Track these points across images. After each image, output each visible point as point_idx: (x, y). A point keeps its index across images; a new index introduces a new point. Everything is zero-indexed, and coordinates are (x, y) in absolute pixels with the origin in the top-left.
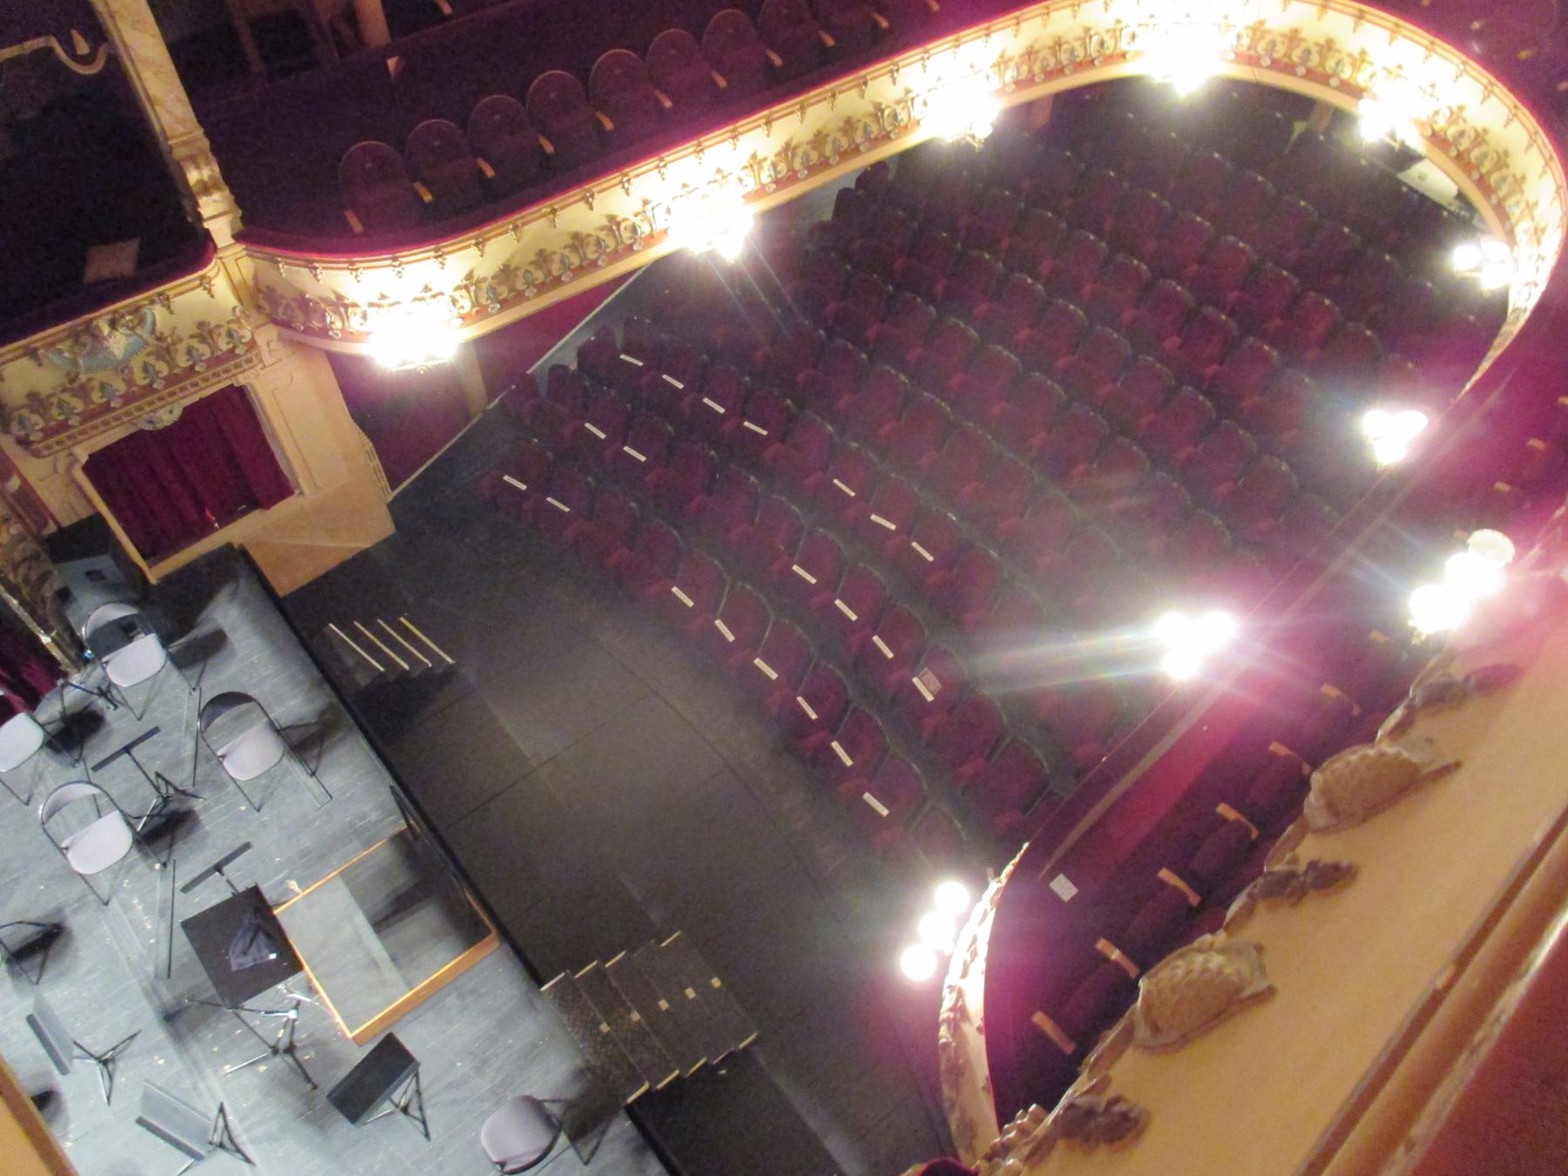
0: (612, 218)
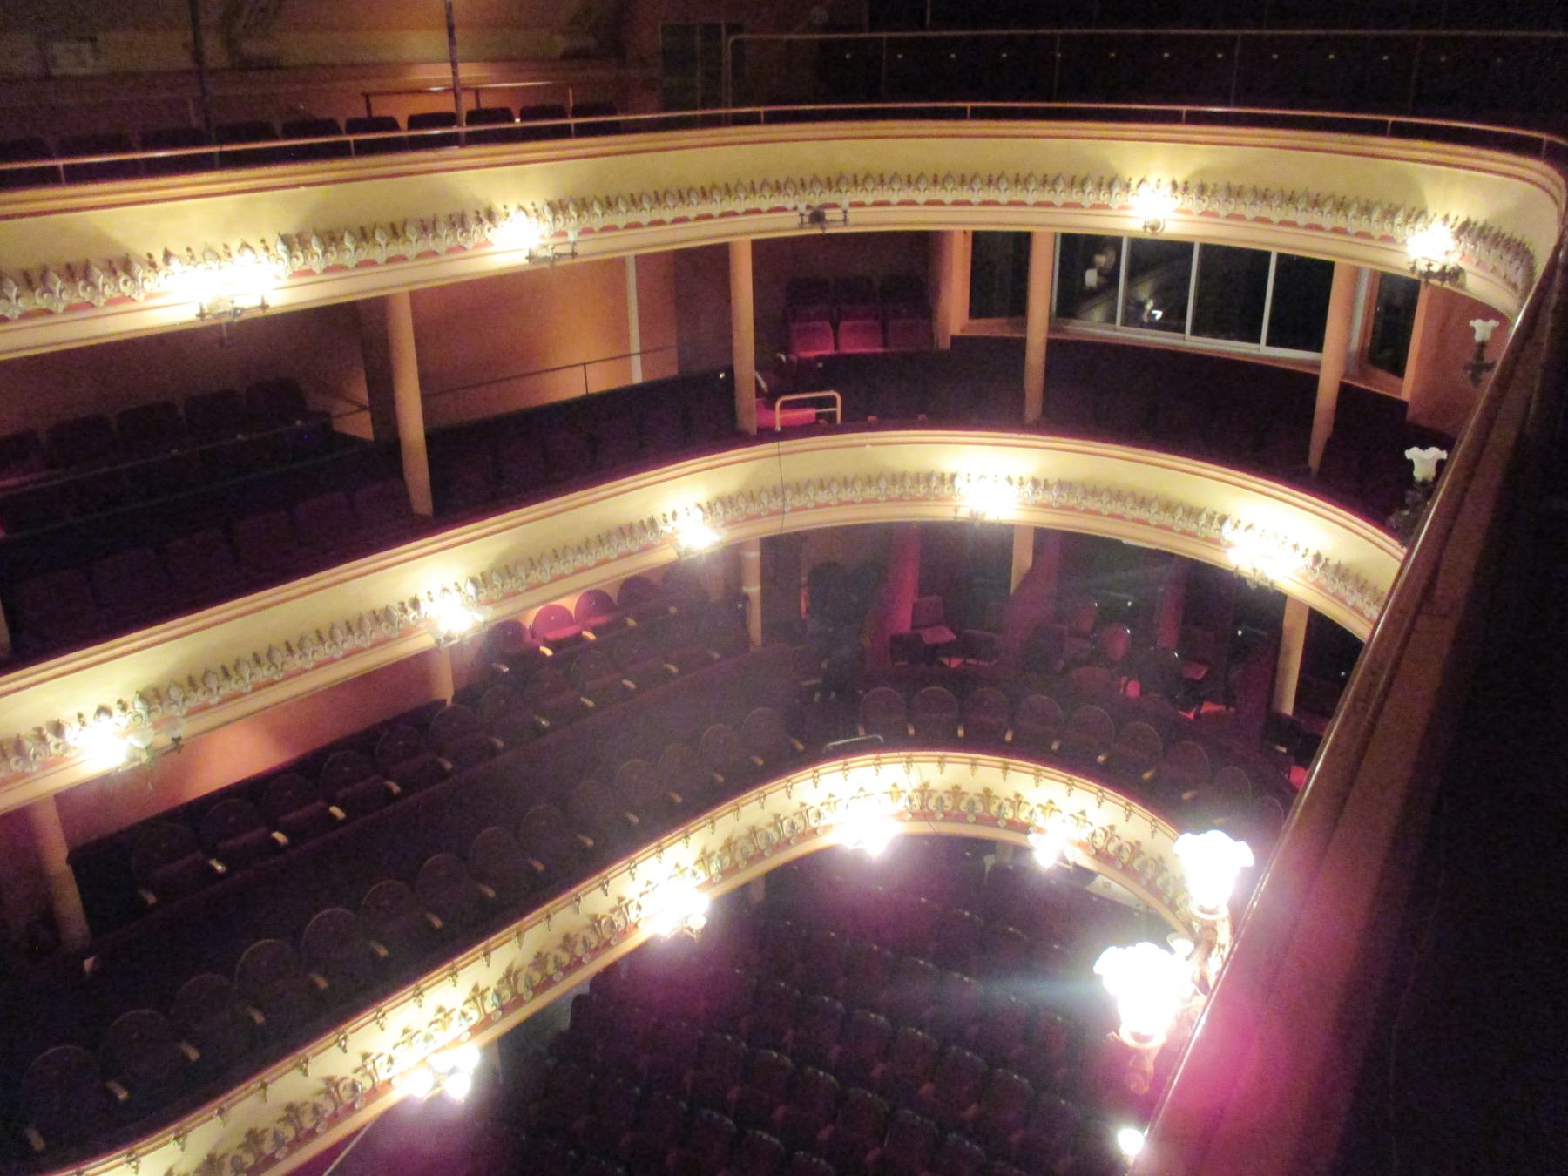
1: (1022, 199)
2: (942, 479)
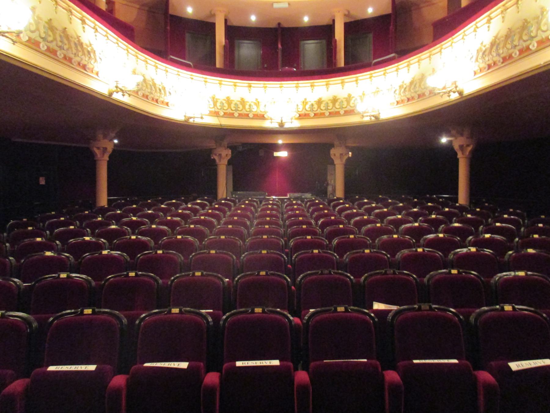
0: (349, 96)
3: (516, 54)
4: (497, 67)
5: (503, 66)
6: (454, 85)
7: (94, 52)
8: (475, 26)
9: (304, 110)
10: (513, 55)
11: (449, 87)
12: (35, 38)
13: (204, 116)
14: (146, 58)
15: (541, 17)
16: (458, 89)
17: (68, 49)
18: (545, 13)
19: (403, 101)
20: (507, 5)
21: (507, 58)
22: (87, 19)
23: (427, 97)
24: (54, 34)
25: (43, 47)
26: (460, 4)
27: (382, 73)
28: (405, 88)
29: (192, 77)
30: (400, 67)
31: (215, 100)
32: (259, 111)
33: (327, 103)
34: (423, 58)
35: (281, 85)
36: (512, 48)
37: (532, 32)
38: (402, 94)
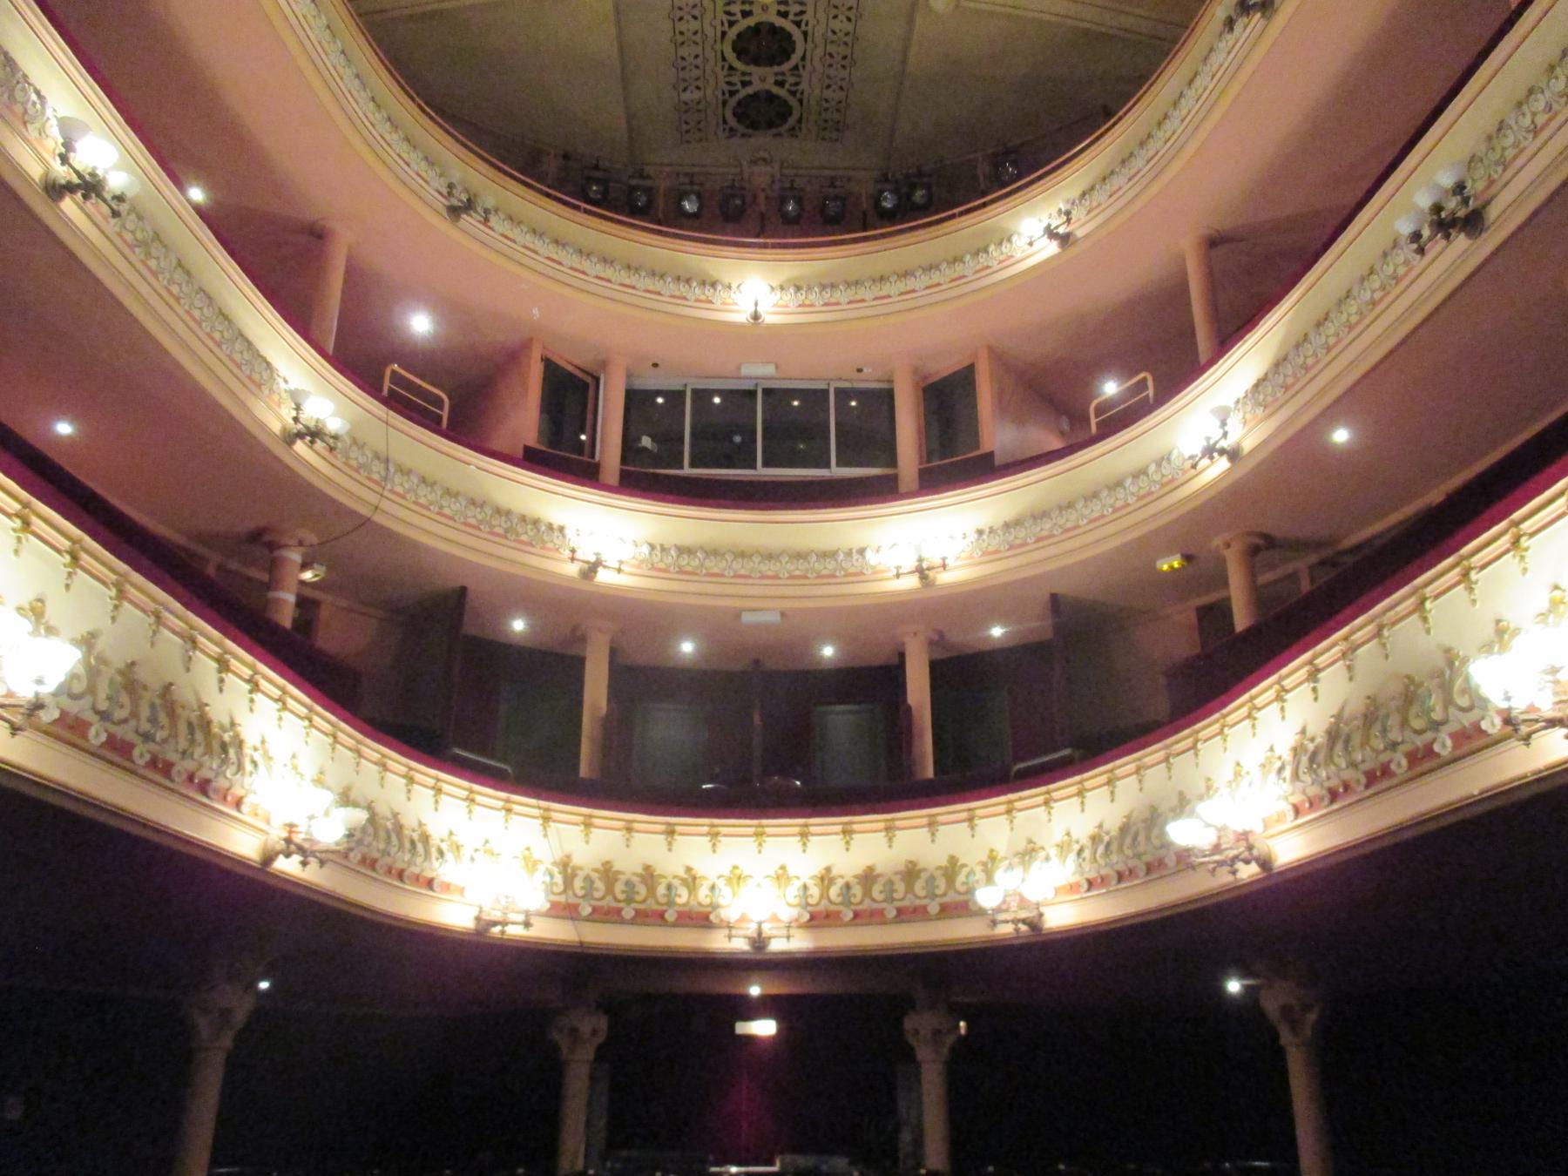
0: (953, 860)
1: (633, 284)
2: (550, 527)
3: (1399, 765)
4: (1354, 798)
5: (1368, 797)
6: (1244, 844)
7: (239, 744)
8: (1277, 687)
9: (824, 902)
10: (1393, 767)
11: (1228, 846)
12: (79, 712)
13: (533, 920)
14: (384, 756)
15: (1448, 672)
16: (1255, 852)
17: (165, 741)
18: (1457, 663)
19: (1104, 880)
20: (1354, 637)
21: (1378, 774)
22: (237, 657)
23: (1170, 872)
24: (135, 702)
25: (97, 734)
26: (1231, 625)
27: (1041, 799)
28: (1108, 845)
29: (508, 805)
30: (1088, 784)
31: (569, 870)
32: (695, 903)
33: (890, 882)
34: (1149, 764)
35: (760, 829)
36: (1385, 749)
37: (1432, 710)
38: (1102, 861)
